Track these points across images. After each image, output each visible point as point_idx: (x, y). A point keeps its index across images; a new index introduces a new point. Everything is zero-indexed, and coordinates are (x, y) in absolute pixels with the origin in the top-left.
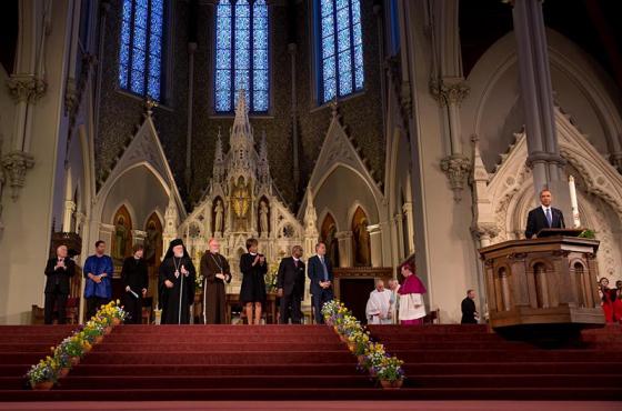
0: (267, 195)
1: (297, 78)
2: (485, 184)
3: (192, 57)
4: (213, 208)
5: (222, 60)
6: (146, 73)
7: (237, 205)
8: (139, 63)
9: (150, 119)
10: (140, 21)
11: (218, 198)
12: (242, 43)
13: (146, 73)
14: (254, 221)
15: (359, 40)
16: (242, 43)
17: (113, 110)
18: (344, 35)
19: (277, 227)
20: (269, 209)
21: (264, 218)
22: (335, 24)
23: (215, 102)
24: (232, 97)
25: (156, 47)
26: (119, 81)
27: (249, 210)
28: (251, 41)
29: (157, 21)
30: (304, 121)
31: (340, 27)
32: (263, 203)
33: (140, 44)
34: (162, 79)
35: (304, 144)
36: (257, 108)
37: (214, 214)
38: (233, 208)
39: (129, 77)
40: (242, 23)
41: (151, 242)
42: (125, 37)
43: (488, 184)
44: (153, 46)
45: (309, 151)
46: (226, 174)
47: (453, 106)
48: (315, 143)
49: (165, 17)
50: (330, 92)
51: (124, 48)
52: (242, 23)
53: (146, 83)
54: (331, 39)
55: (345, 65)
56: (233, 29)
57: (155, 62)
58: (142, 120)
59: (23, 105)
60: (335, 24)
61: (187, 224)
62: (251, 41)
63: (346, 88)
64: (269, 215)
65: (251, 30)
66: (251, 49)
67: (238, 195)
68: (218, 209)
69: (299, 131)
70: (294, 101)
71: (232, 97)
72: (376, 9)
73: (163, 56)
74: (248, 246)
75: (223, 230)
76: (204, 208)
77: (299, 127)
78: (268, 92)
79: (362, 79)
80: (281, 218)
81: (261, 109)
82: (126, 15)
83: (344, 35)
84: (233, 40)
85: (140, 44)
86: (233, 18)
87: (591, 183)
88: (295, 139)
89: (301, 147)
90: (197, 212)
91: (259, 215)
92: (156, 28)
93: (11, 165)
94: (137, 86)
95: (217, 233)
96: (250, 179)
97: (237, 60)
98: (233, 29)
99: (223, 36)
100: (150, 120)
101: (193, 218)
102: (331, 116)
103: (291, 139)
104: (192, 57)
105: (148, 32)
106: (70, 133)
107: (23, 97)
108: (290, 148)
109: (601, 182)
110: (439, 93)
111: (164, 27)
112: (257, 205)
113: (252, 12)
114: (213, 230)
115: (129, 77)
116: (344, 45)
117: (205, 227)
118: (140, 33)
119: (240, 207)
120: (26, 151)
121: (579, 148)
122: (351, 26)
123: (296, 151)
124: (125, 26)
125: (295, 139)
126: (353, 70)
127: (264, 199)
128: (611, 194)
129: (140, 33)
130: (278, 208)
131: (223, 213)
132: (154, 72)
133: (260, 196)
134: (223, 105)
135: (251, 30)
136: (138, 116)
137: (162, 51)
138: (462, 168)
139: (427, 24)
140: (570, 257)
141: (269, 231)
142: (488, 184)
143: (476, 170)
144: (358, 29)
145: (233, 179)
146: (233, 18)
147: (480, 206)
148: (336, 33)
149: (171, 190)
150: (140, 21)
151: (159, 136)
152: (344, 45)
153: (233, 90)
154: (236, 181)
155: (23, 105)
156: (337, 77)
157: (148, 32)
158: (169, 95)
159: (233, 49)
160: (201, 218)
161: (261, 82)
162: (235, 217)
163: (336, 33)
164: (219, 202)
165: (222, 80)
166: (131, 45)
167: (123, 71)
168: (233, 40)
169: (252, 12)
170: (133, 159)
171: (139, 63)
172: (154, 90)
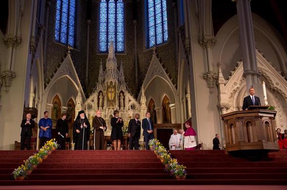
0: (123, 90)
1: (137, 36)
2: (224, 85)
3: (89, 26)
4: (98, 96)
5: (103, 28)
6: (67, 34)
7: (110, 95)
8: (64, 29)
9: (69, 55)
10: (65, 10)
11: (101, 92)
12: (112, 20)
13: (67, 34)
14: (117, 102)
15: (165, 19)
16: (112, 20)
17: (52, 51)
18: (159, 16)
19: (128, 105)
20: (124, 97)
21: (122, 101)
22: (155, 11)
23: (99, 47)
24: (107, 45)
25: (72, 22)
26: (55, 37)
27: (115, 97)
28: (116, 19)
29: (72, 10)
30: (140, 56)
31: (157, 12)
32: (121, 94)
33: (64, 20)
34: (75, 36)
35: (140, 67)
36: (118, 50)
37: (99, 99)
38: (107, 96)
39: (60, 36)
40: (112, 11)
41: (69, 112)
42: (58, 17)
43: (225, 85)
44: (70, 21)
45: (143, 70)
46: (104, 81)
47: (209, 49)
48: (145, 66)
49: (76, 8)
50: (152, 43)
51: (57, 22)
52: (112, 11)
53: (67, 38)
54: (153, 18)
55: (159, 30)
56: (108, 13)
57: (71, 29)
58: (66, 56)
59: (11, 48)
60: (155, 11)
61: (86, 103)
62: (116, 19)
63: (160, 41)
64: (124, 99)
65: (116, 14)
66: (116, 23)
67: (110, 90)
68: (101, 97)
69: (138, 61)
70: (136, 47)
71: (107, 45)
72: (173, 4)
73: (75, 26)
74: (115, 114)
75: (103, 106)
76: (94, 96)
77: (138, 59)
78: (124, 42)
79: (167, 37)
80: (130, 101)
81: (120, 50)
82: (58, 7)
83: (159, 16)
84: (108, 19)
85: (64, 20)
86: (108, 8)
87: (273, 84)
88: (136, 64)
89: (139, 68)
90: (91, 98)
91: (119, 100)
92: (72, 13)
93: (5, 76)
94: (63, 40)
95: (100, 108)
96: (115, 83)
97: (109, 28)
98: (108, 13)
99: (103, 17)
100: (69, 56)
101: (89, 101)
102: (153, 54)
103: (134, 64)
104: (89, 26)
105: (68, 15)
106: (32, 61)
107: (11, 45)
108: (134, 69)
109: (277, 84)
110: (203, 43)
111: (76, 13)
112: (118, 95)
113: (116, 6)
114: (98, 106)
115: (60, 36)
116: (159, 21)
117: (95, 105)
118: (65, 15)
119: (111, 96)
120: (12, 70)
121: (267, 69)
122: (162, 12)
123: (136, 70)
124: (58, 12)
125: (136, 64)
126: (163, 33)
127: (122, 92)
128: (282, 89)
129: (65, 15)
130: (128, 96)
131: (103, 99)
132: (71, 33)
133: (120, 91)
134: (103, 48)
135: (116, 14)
136: (64, 54)
137: (75, 23)
138: (213, 78)
139: (197, 11)
140: (263, 119)
141: (124, 107)
142: (225, 85)
143: (220, 79)
144: (165, 13)
145: (107, 83)
146: (108, 8)
147: (222, 95)
148: (155, 15)
149: (79, 88)
150: (65, 10)
151: (73, 63)
152: (159, 21)
153: (107, 41)
154: (109, 84)
155: (11, 48)
156: (156, 35)
157: (68, 15)
158: (78, 44)
159: (107, 23)
160: (93, 101)
161: (120, 38)
162: (108, 100)
163: (155, 15)
164: (101, 94)
165: (103, 37)
166: (60, 21)
167: (57, 33)
168: (108, 19)
169: (116, 6)
170: (61, 74)
171: (64, 29)
172: (71, 42)
